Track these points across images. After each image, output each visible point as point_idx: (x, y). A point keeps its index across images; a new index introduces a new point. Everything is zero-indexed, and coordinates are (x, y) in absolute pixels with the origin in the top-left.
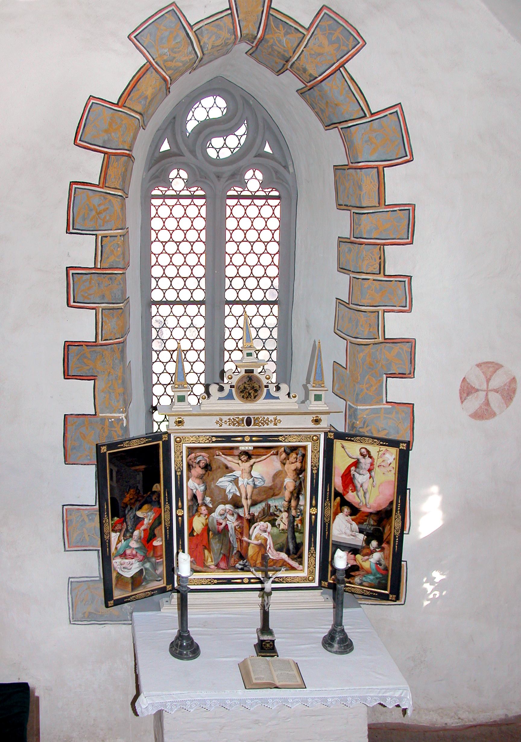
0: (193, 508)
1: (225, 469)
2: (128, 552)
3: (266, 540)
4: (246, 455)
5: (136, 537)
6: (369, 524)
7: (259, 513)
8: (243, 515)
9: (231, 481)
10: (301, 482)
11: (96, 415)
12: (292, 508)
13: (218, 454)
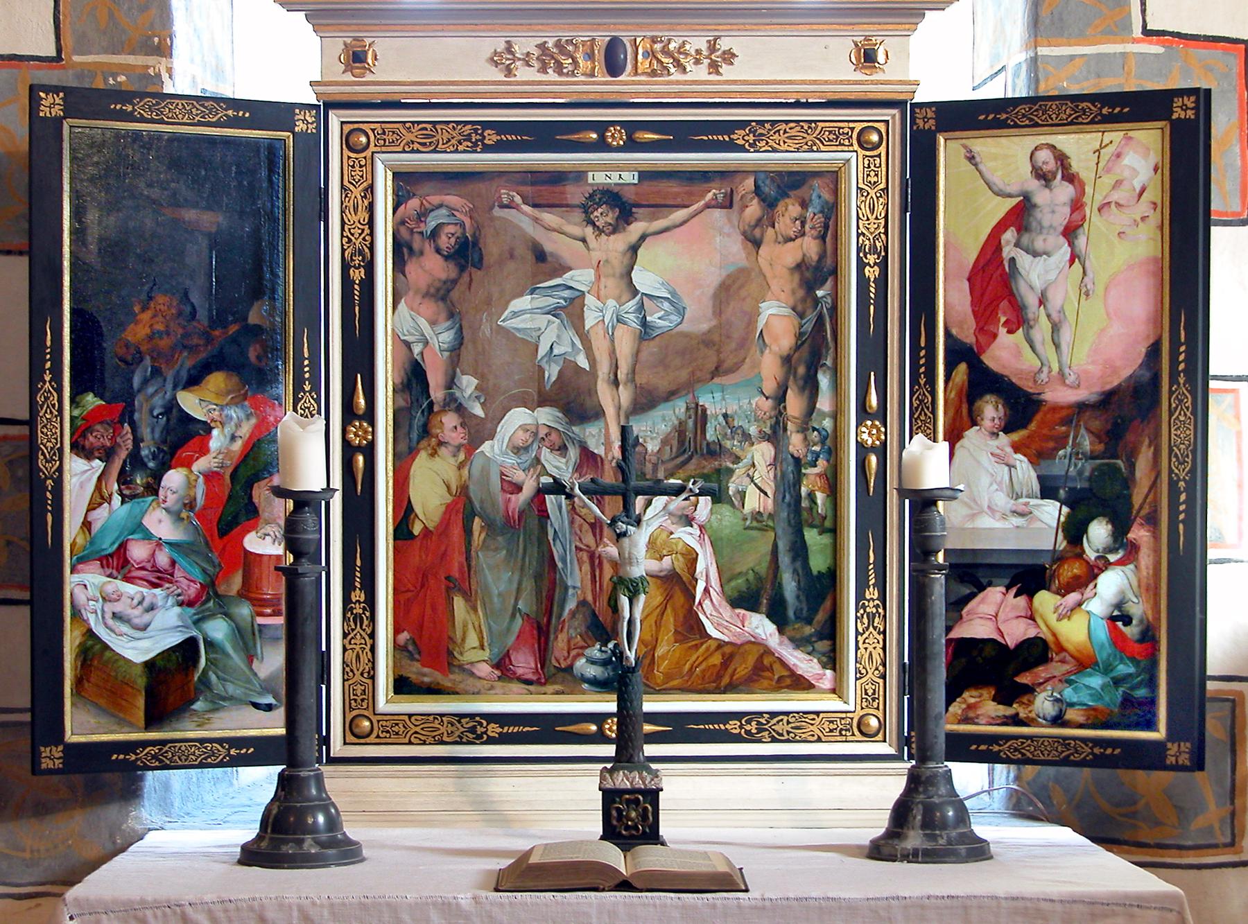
0: (412, 418)
1: (530, 257)
2: (138, 552)
3: (691, 559)
4: (612, 207)
5: (171, 499)
6: (1076, 454)
7: (665, 442)
8: (600, 451)
9: (554, 312)
10: (820, 317)
11: (58, 58)
12: (790, 426)
13: (505, 201)
